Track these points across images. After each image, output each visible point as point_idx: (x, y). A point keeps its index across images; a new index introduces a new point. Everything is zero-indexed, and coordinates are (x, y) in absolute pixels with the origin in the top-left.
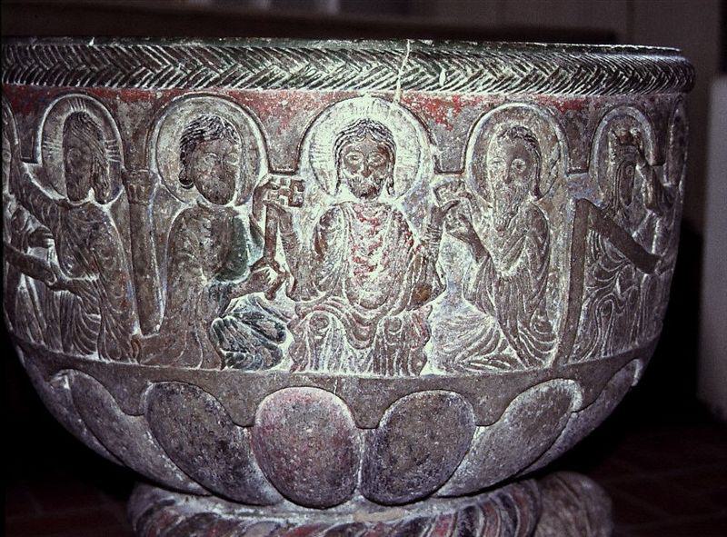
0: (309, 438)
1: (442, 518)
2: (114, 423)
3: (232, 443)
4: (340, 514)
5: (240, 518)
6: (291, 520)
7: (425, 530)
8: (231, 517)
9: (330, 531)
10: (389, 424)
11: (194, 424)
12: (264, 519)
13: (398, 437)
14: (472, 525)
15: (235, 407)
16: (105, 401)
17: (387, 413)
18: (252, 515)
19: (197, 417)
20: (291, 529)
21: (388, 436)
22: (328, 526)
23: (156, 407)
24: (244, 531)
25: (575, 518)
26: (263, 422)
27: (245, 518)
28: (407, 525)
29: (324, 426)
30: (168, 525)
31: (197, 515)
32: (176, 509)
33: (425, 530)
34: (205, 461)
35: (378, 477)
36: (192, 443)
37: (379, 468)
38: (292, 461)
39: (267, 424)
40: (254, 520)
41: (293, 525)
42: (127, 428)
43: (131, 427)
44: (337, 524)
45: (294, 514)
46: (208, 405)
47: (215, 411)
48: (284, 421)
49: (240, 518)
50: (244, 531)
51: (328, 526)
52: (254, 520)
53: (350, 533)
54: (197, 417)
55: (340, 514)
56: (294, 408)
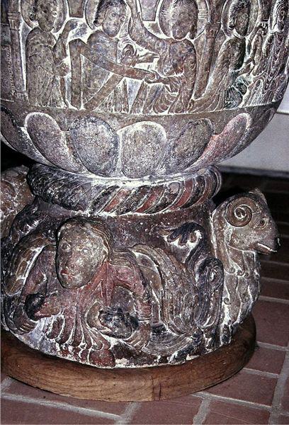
8: (155, 185)
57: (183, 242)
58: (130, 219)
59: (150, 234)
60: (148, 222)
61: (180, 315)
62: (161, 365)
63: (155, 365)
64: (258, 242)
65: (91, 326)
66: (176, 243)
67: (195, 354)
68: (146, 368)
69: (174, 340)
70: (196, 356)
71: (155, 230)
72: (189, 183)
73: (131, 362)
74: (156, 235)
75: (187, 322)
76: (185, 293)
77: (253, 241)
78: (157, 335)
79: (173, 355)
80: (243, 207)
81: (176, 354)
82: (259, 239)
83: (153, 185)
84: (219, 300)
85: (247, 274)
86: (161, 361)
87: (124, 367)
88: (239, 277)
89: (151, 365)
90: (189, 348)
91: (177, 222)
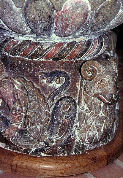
0: (77, 14)
1: (95, 39)
2: (11, 11)
3: (52, 16)
4: (69, 39)
5: (39, 41)
6: (56, 41)
7: (92, 43)
8: (36, 41)
9: (68, 44)
10: (100, 9)
11: (42, 10)
12: (47, 41)
13: (102, 13)
14: (102, 41)
15: (57, 5)
16: (10, 4)
17: (100, 6)
18: (43, 40)
19: (44, 8)
20: (56, 44)
21: (99, 13)
22: (67, 42)
23: (29, 5)
24: (42, 45)
25: (42, 49)
26: (64, 9)
27: (40, 41)
28: (87, 42)
29: (83, 10)
30: (15, 44)
31: (25, 41)
32: (15, 39)
33: (92, 43)
34: (42, 22)
35: (90, 26)
36: (39, 17)
37: (92, 23)
38: (70, 21)
39: (65, 10)
40: (44, 42)
41: (57, 43)
42: (16, 12)
43: (17, 12)
44: (69, 42)
45: (56, 39)
46: (48, 4)
47: (50, 6)
48: (71, 8)
49: (39, 41)
50: (42, 45)
51: (67, 42)
52: (44, 42)
53: (74, 44)
54: (44, 8)
55: (69, 39)
56: (75, 4)
57: (50, 82)
58: (20, 60)
59: (31, 72)
60: (30, 65)
61: (34, 127)
62: (24, 153)
63: (21, 152)
64: (99, 94)
65: (72, 136)
66: (45, 81)
67: (48, 154)
68: (15, 152)
69: (31, 141)
70: (49, 156)
71: (34, 71)
72: (61, 44)
73: (7, 146)
74: (35, 73)
75: (38, 133)
76: (38, 114)
77: (96, 92)
78: (20, 135)
79: (33, 150)
80: (91, 67)
81: (34, 150)
82: (100, 91)
83: (34, 41)
84: (115, 132)
85: (92, 113)
86: (25, 151)
87: (4, 148)
88: (87, 114)
89: (19, 152)
90: (42, 149)
91: (50, 69)
